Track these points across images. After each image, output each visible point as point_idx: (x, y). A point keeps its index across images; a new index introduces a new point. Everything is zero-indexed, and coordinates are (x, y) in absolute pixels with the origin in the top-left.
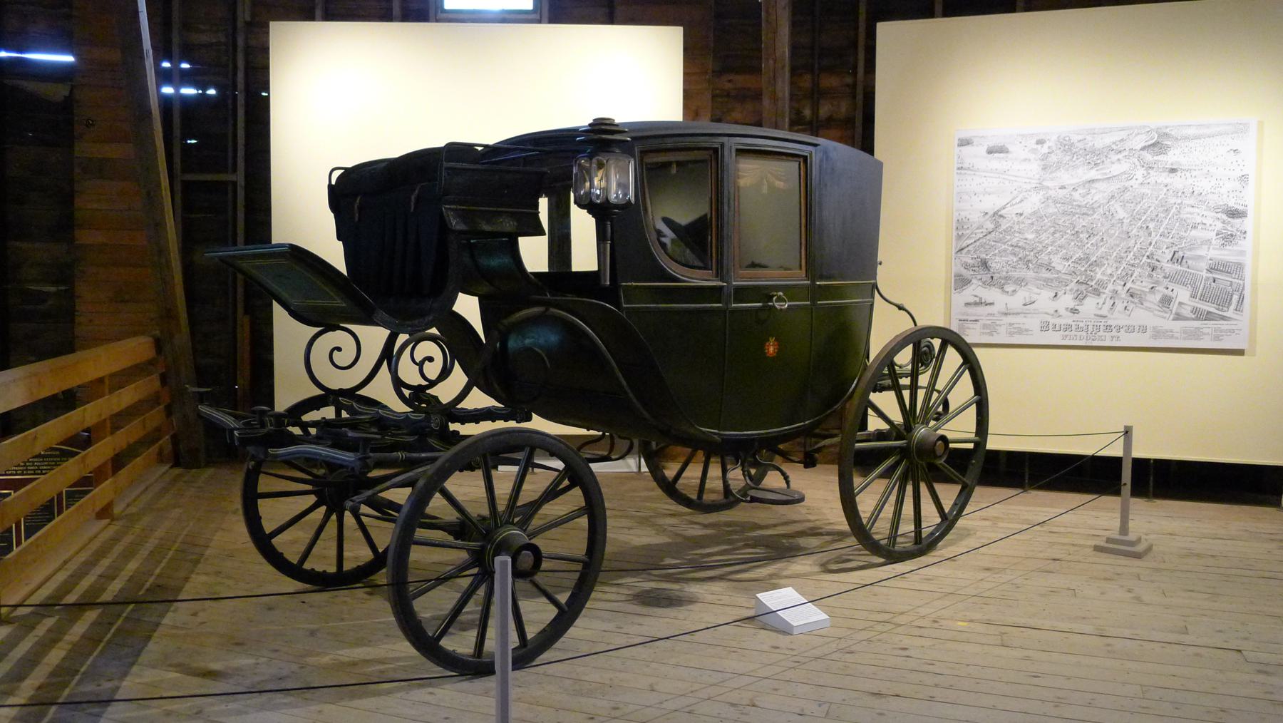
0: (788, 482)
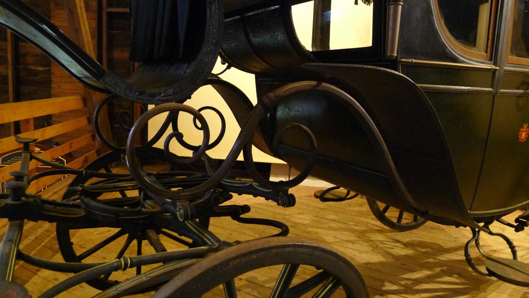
0: (514, 252)
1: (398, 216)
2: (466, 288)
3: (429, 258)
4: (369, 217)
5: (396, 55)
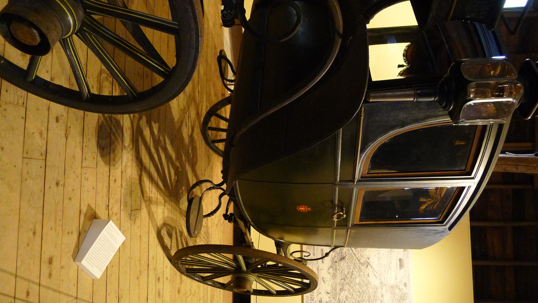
1: (213, 127)
2: (169, 187)
3: (185, 156)
4: (208, 103)
5: (371, 101)
